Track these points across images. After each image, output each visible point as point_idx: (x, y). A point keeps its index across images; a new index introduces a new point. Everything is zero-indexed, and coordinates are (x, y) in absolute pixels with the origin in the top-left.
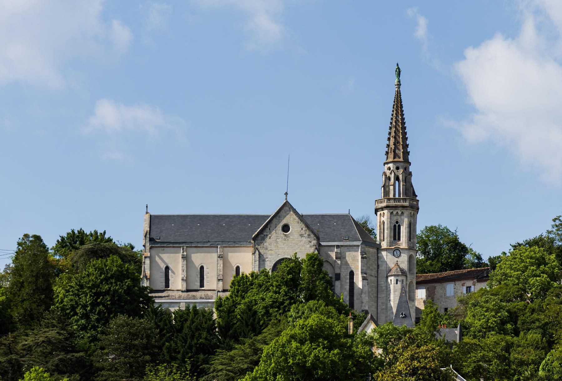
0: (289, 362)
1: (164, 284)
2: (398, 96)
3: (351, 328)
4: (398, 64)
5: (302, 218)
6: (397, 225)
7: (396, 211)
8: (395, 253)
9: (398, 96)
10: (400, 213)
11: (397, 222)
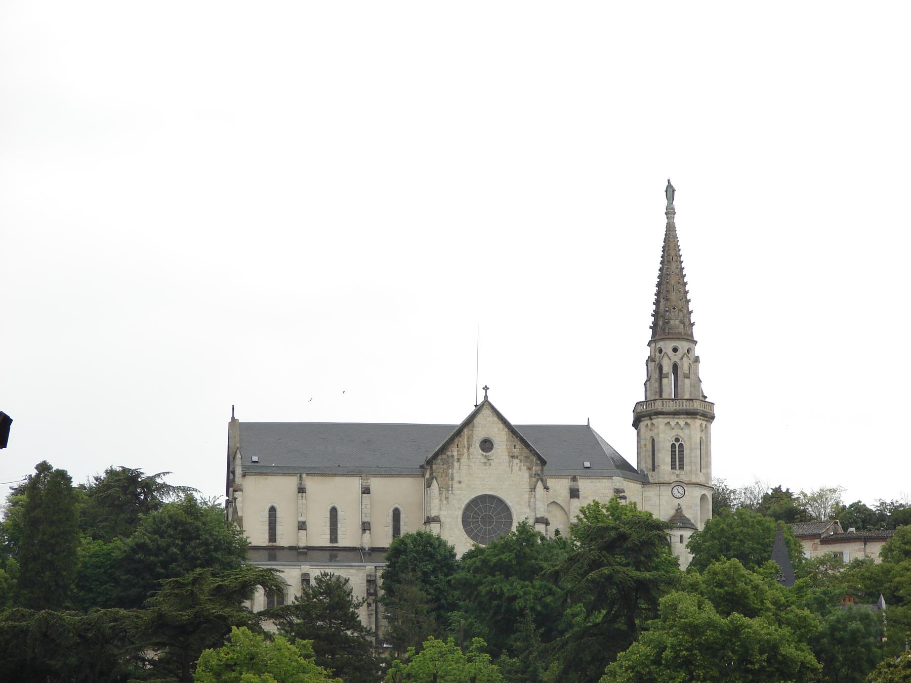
0: (371, 642)
1: (267, 536)
2: (671, 230)
3: (337, 573)
4: (669, 180)
5: (512, 430)
6: (677, 444)
7: (677, 420)
8: (675, 491)
9: (671, 230)
10: (682, 423)
11: (677, 440)
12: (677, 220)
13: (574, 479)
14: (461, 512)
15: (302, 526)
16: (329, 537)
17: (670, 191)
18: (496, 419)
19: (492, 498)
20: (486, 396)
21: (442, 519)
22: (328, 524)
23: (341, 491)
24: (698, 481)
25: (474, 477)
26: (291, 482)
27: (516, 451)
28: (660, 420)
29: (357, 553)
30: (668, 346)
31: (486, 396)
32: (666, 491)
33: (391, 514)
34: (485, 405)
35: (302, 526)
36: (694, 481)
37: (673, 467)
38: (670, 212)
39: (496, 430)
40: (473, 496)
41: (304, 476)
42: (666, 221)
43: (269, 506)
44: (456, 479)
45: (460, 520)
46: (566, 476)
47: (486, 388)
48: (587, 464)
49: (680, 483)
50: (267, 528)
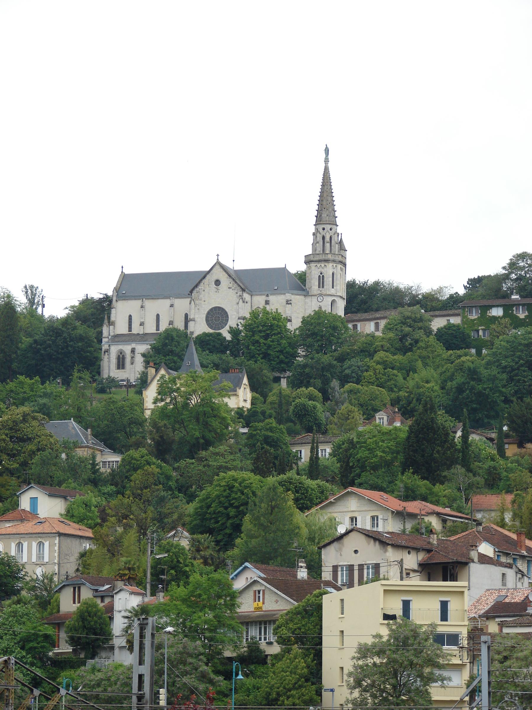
1: (127, 329)
2: (326, 169)
6: (321, 276)
8: (319, 298)
9: (326, 169)
10: (323, 265)
11: (321, 273)
12: (330, 165)
13: (267, 296)
14: (205, 316)
15: (142, 324)
16: (155, 328)
17: (327, 151)
18: (222, 270)
19: (219, 308)
20: (218, 259)
21: (196, 320)
22: (155, 322)
23: (160, 306)
24: (330, 293)
25: (210, 298)
26: (138, 303)
27: (231, 285)
28: (312, 264)
29: (142, 338)
30: (320, 227)
31: (218, 259)
32: (314, 299)
33: (184, 316)
34: (218, 263)
35: (142, 324)
36: (328, 294)
37: (319, 287)
38: (327, 161)
39: (222, 275)
40: (211, 308)
41: (144, 300)
42: (324, 165)
43: (129, 314)
44: (203, 300)
45: (204, 319)
46: (264, 295)
47: (218, 255)
48: (276, 288)
49: (321, 295)
50: (128, 325)
